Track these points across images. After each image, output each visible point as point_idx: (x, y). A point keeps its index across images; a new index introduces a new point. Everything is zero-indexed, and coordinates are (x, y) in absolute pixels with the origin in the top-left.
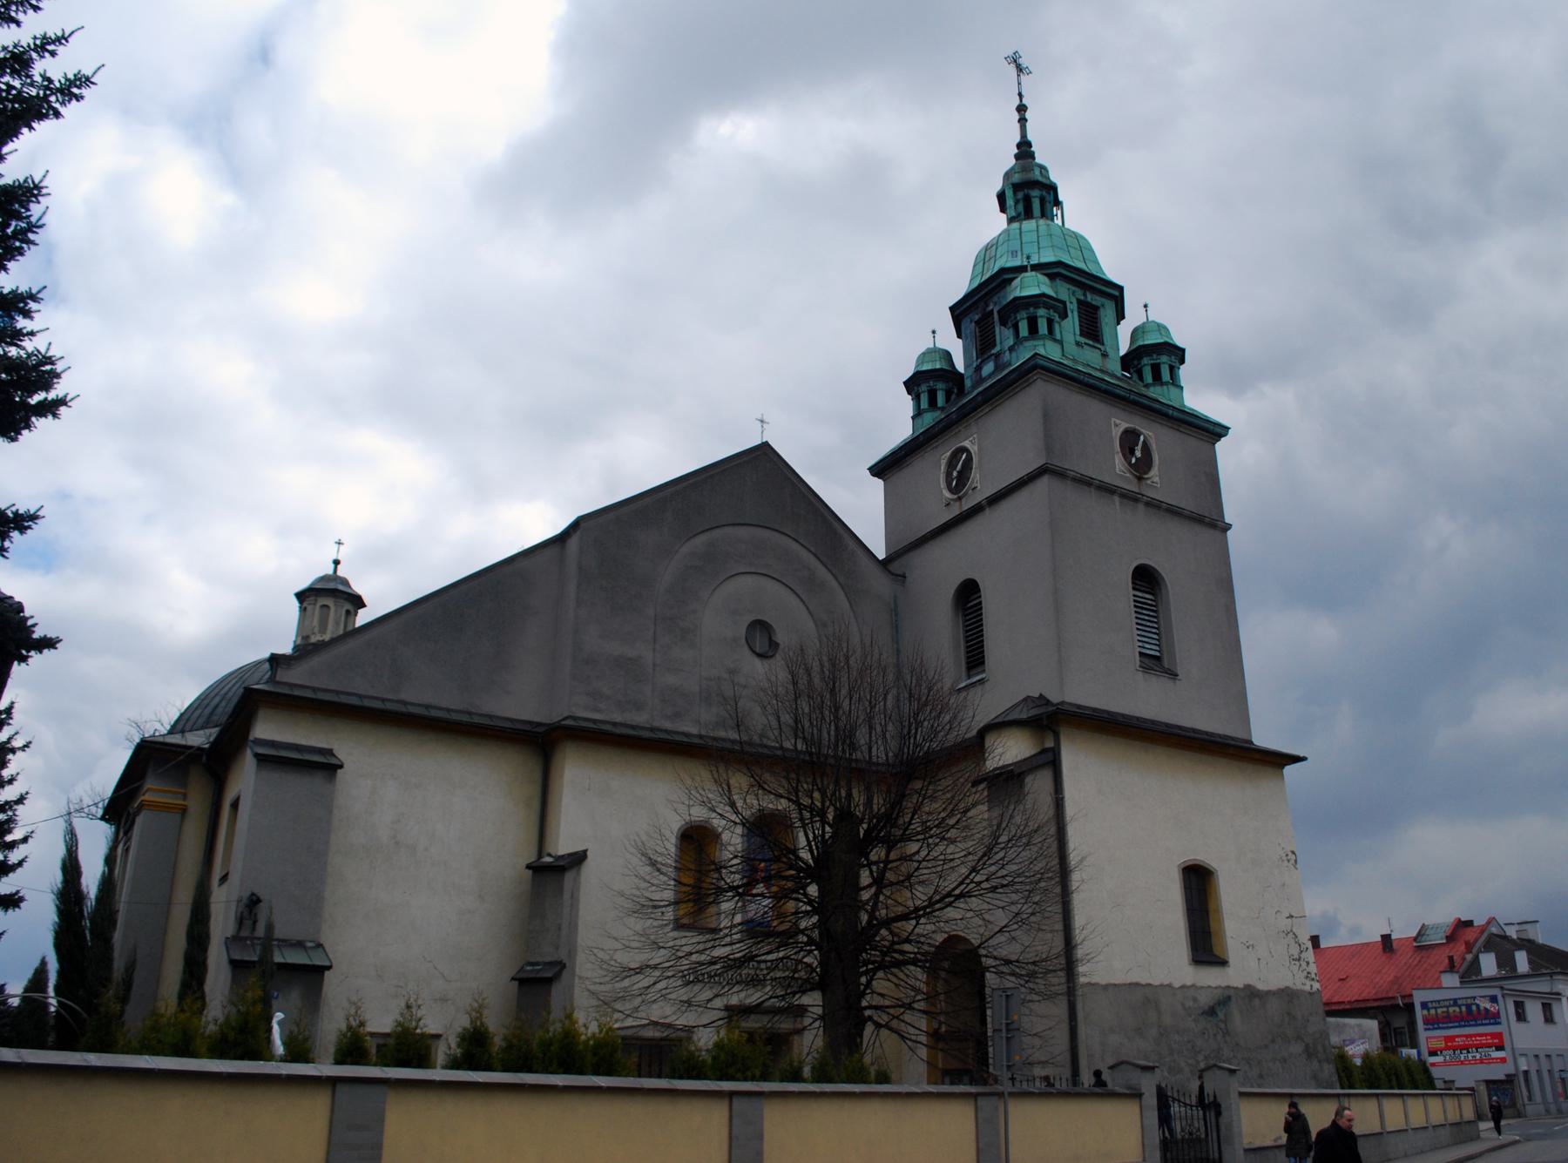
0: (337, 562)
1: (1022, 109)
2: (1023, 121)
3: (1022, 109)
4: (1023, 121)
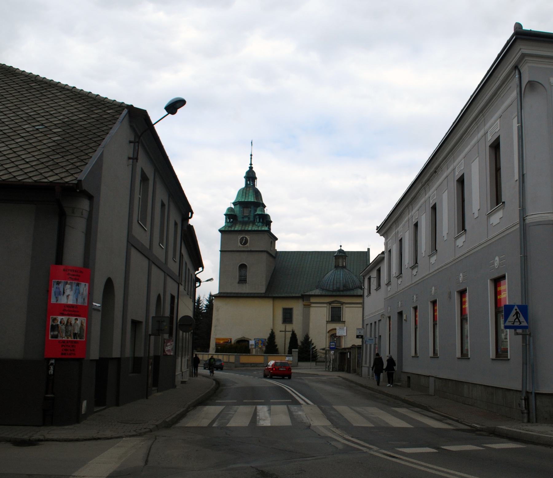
0: (341, 246)
1: (251, 155)
2: (251, 158)
3: (251, 155)
4: (251, 158)
